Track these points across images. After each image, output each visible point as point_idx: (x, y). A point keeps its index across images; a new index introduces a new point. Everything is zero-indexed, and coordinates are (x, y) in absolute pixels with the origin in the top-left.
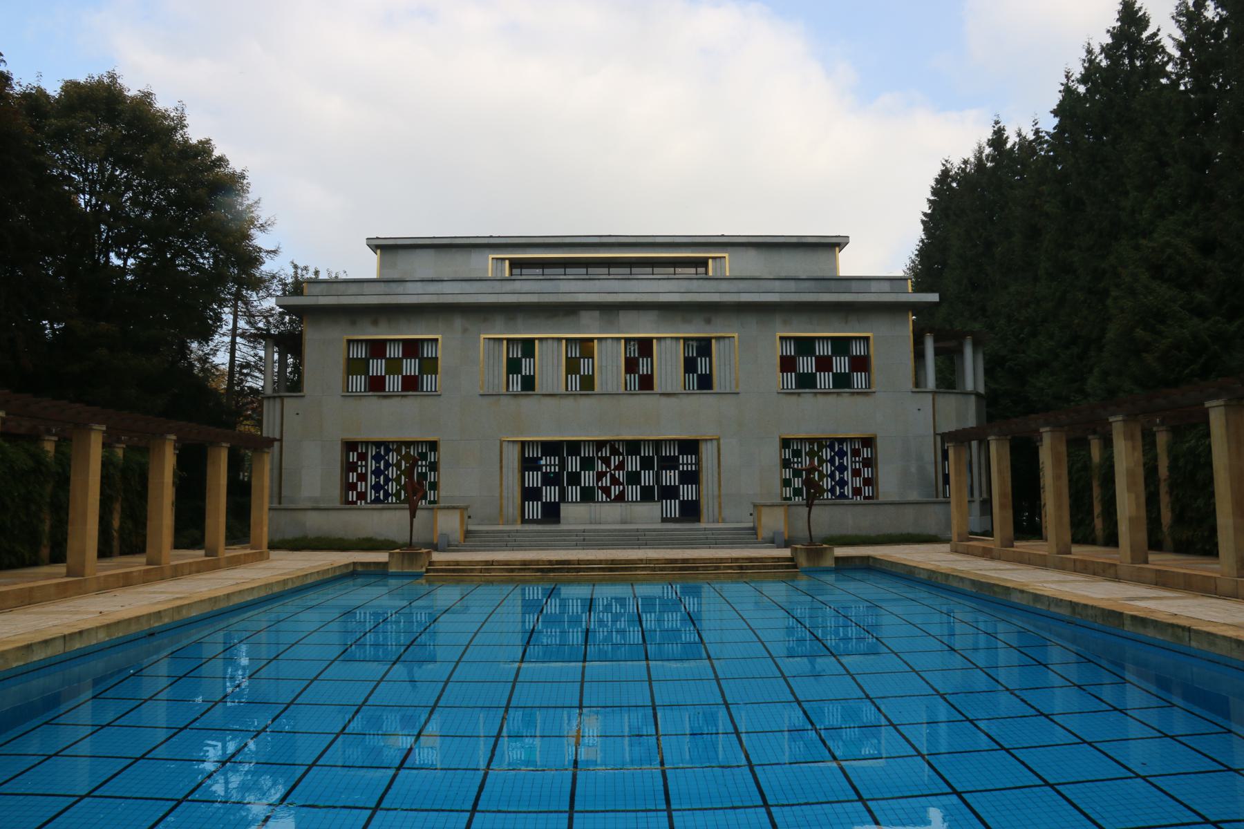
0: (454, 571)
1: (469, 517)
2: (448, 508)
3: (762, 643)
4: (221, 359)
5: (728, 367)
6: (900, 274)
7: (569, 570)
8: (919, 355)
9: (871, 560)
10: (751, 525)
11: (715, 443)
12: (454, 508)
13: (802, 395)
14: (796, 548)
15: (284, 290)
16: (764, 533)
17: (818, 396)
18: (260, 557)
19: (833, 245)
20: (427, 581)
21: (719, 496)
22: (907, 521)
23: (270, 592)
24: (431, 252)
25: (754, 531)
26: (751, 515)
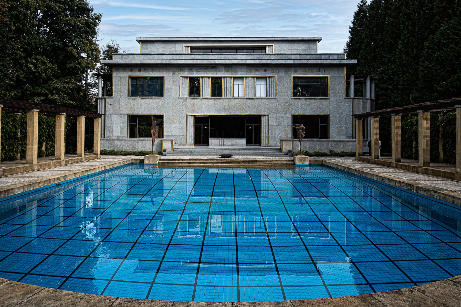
1: (175, 143)
5: (272, 88)
6: (342, 51)
8: (348, 84)
10: (280, 148)
11: (267, 117)
18: (97, 158)
19: (315, 41)
20: (159, 166)
21: (268, 137)
22: (340, 149)
25: (280, 150)
26: (280, 144)
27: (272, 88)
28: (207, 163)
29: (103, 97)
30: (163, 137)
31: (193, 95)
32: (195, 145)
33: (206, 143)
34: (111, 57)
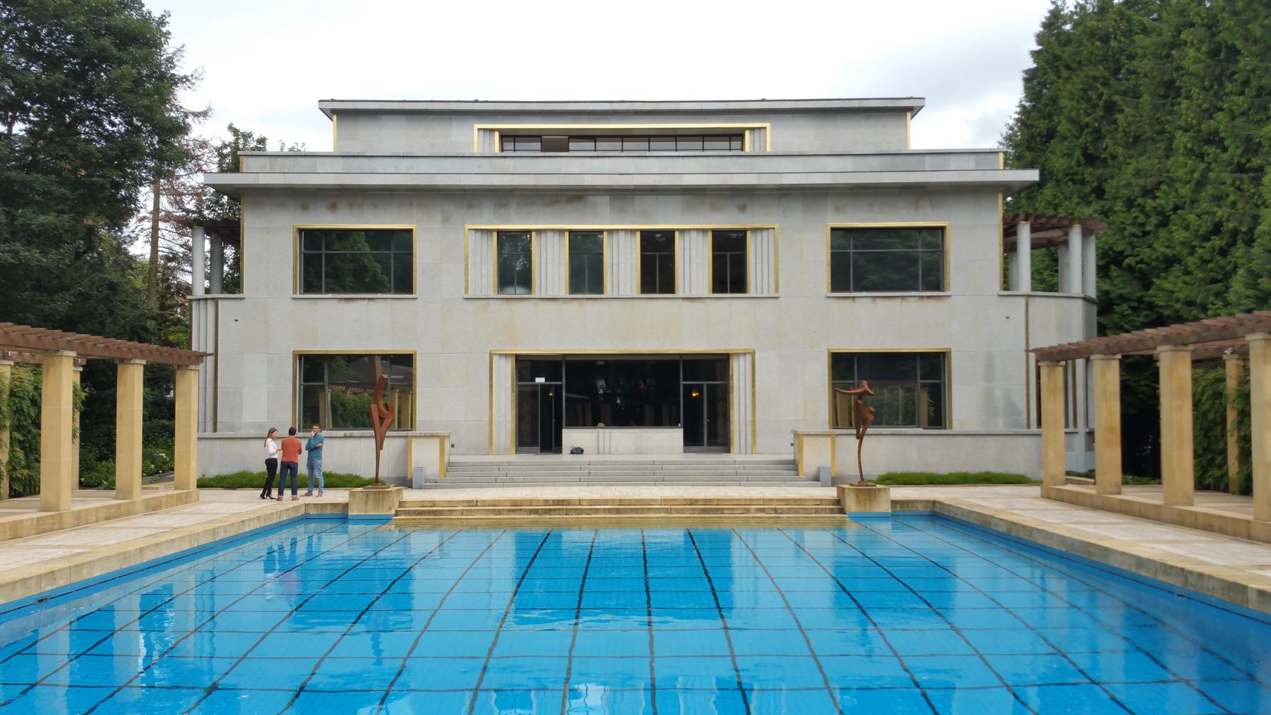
0: (429, 512)
1: (453, 446)
2: (425, 436)
3: (772, 579)
4: (140, 249)
7: (568, 512)
8: (1010, 248)
9: (937, 505)
10: (791, 457)
11: (749, 358)
12: (432, 436)
13: (857, 300)
14: (843, 489)
15: (220, 164)
16: (808, 466)
17: (877, 300)
18: (183, 500)
19: (900, 111)
20: (397, 526)
22: (988, 458)
23: (196, 545)
24: (403, 118)
25: (794, 466)
26: (792, 445)
27: (765, 265)
28: (625, 511)
29: (208, 296)
30: (412, 427)
31: (511, 290)
32: (517, 452)
33: (551, 444)
34: (235, 168)
